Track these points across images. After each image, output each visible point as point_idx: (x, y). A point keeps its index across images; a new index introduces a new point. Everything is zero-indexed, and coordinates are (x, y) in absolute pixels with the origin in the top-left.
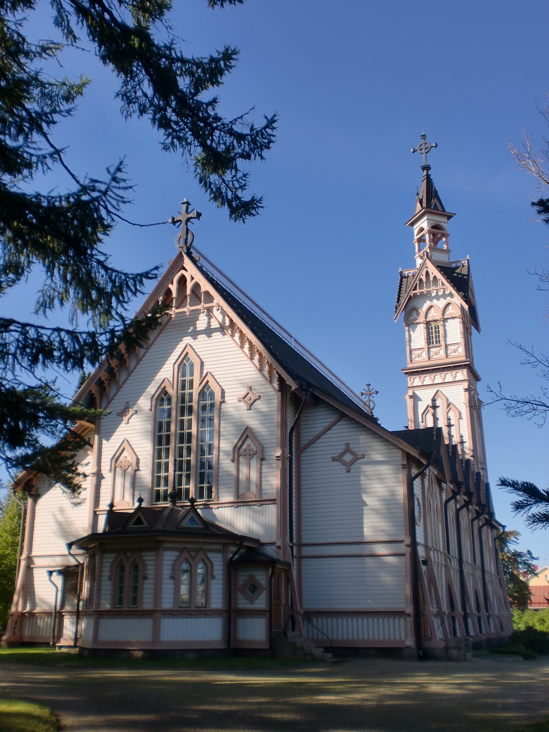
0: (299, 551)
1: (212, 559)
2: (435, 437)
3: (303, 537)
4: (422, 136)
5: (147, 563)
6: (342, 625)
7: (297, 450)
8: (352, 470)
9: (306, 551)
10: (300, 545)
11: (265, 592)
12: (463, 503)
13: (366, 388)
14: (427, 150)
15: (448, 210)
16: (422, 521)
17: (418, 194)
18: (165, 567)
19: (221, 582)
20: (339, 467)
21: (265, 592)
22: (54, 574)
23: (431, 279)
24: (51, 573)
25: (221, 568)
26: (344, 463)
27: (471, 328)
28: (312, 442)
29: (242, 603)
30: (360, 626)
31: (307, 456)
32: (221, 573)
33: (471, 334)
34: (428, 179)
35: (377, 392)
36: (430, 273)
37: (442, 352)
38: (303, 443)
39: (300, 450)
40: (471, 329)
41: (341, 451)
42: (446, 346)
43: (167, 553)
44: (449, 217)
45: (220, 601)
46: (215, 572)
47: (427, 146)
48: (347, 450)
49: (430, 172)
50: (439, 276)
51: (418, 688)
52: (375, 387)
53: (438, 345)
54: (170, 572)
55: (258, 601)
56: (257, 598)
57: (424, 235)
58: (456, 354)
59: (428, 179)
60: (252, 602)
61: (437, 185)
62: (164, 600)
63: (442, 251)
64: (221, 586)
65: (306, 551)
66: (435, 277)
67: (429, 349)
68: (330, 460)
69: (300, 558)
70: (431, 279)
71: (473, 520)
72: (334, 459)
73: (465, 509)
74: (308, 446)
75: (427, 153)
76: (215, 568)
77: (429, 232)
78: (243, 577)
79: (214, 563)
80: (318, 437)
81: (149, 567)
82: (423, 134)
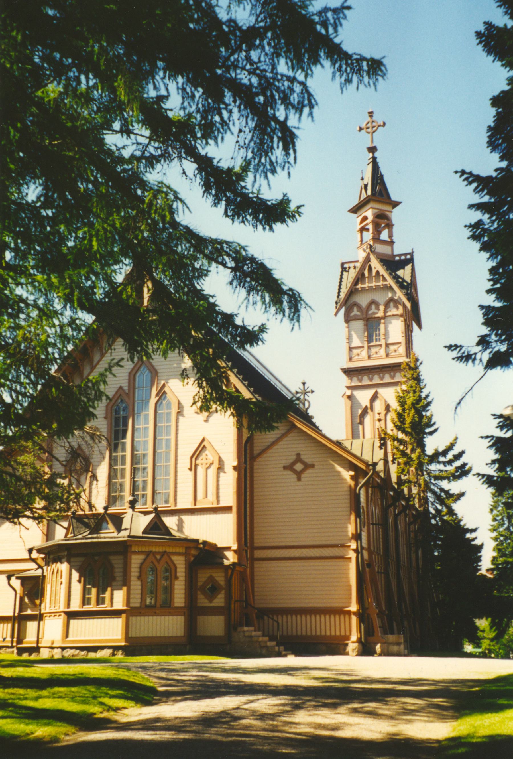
0: (252, 554)
1: (176, 562)
2: (8, 160)
3: (255, 541)
4: (369, 113)
5: (115, 566)
6: (287, 622)
7: (250, 459)
8: (303, 479)
9: (258, 554)
10: (254, 548)
11: (223, 592)
12: (401, 509)
13: (301, 386)
14: (374, 129)
15: (394, 197)
16: (366, 527)
17: (362, 179)
18: (132, 570)
19: (183, 583)
20: (291, 476)
21: (223, 592)
22: (13, 578)
23: (374, 274)
24: (9, 578)
25: (184, 570)
26: (295, 472)
27: (412, 324)
28: (264, 451)
29: (203, 601)
30: (299, 621)
31: (258, 465)
32: (184, 574)
33: (412, 331)
34: (375, 163)
35: (312, 392)
36: (373, 267)
37: (382, 352)
38: (256, 452)
39: (253, 458)
40: (412, 327)
41: (291, 461)
42: (387, 345)
43: (134, 557)
44: (395, 204)
45: (183, 600)
46: (178, 574)
47: (374, 124)
48: (298, 459)
49: (376, 154)
50: (383, 271)
51: (292, 700)
52: (310, 386)
53: (378, 343)
54: (137, 574)
55: (216, 601)
56: (215, 598)
57: (367, 224)
58: (397, 353)
59: (375, 163)
60: (211, 602)
61: (384, 170)
62: (176, 600)
63: (384, 242)
64: (183, 587)
65: (258, 554)
66: (378, 272)
67: (369, 347)
68: (282, 469)
69: (253, 559)
70: (374, 274)
71: (410, 524)
72: (285, 468)
73: (403, 514)
74: (260, 455)
75: (374, 132)
76: (178, 570)
77: (373, 222)
78: (203, 576)
79: (178, 566)
80: (269, 447)
81: (117, 570)
82: (370, 111)
